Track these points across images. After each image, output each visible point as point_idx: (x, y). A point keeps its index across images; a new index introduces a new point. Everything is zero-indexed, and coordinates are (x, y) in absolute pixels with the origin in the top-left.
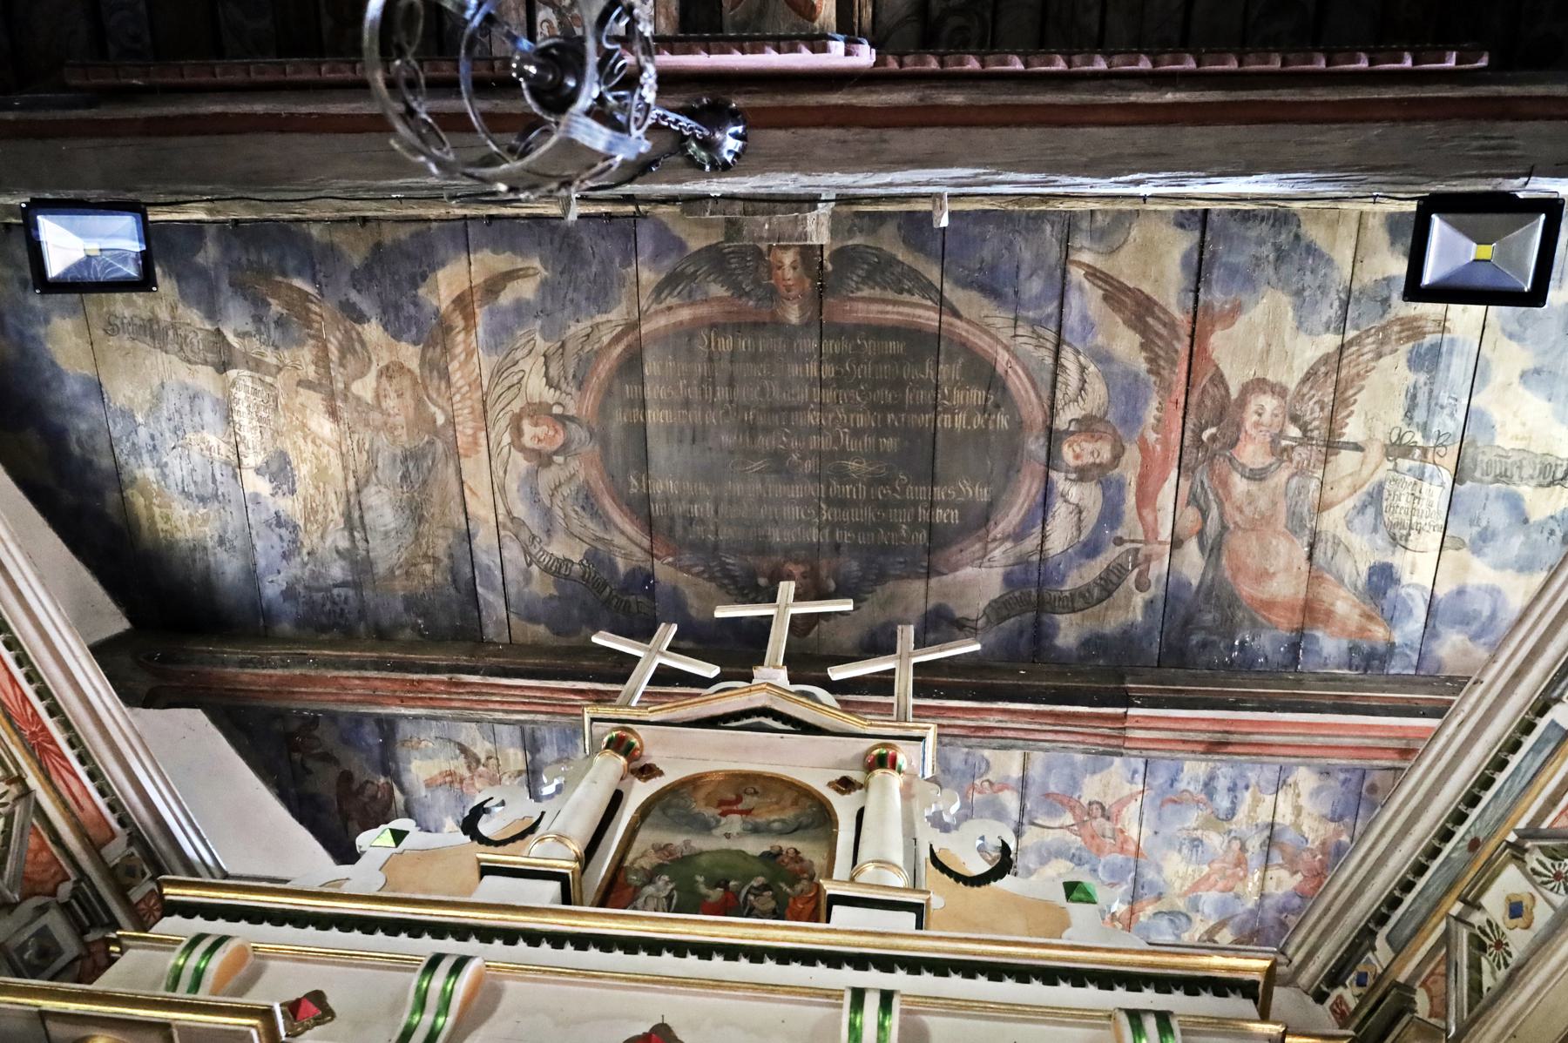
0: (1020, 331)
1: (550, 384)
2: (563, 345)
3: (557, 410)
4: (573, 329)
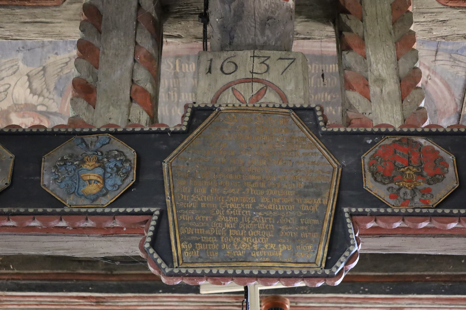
0: (439, 58)
1: (33, 92)
2: (44, 69)
3: (43, 109)
4: (52, 59)
